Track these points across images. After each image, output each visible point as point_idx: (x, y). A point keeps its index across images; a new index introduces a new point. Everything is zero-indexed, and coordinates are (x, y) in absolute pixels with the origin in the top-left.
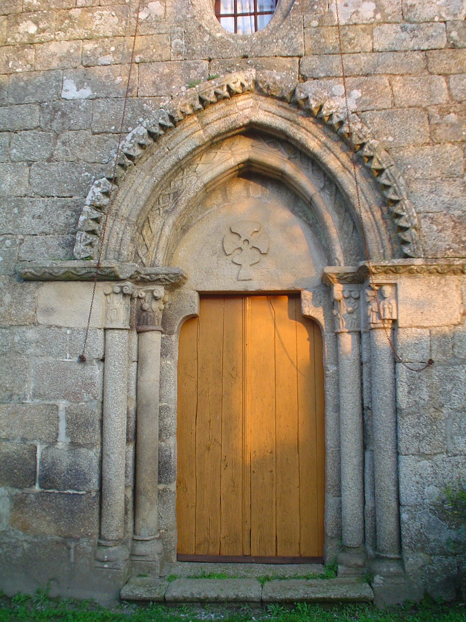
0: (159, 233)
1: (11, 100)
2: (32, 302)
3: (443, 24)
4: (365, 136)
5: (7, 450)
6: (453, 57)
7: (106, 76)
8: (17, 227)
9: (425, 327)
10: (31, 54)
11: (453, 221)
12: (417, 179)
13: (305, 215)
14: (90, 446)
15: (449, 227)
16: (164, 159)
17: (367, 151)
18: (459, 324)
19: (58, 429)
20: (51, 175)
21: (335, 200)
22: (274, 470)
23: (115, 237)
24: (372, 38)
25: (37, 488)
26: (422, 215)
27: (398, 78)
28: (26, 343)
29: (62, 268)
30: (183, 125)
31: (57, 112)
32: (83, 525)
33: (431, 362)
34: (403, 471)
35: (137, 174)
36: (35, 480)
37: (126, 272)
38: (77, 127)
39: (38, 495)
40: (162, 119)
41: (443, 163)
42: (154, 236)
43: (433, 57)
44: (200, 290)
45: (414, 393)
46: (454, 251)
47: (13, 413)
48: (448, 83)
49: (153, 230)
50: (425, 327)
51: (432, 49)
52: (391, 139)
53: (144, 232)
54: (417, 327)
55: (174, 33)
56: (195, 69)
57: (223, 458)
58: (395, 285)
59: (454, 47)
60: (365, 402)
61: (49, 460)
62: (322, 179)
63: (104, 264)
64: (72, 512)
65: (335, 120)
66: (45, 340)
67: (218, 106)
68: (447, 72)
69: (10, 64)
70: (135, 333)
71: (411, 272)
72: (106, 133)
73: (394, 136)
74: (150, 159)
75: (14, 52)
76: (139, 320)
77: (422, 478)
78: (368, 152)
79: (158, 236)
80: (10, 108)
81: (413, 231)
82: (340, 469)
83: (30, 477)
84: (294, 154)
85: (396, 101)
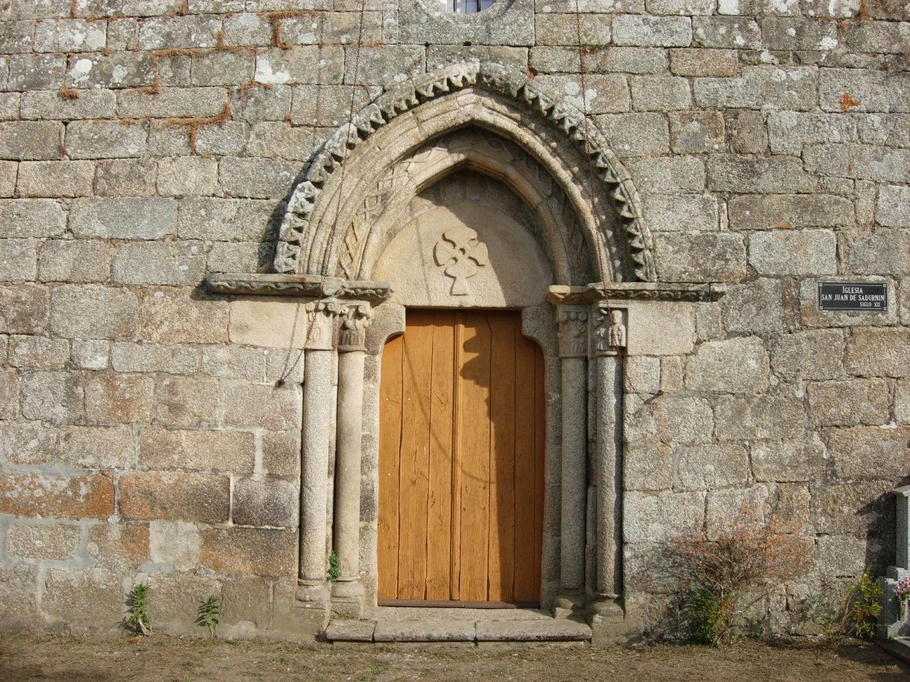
1: (195, 81)
2: (223, 318)
3: (689, 19)
4: (599, 145)
5: (196, 482)
6: (698, 58)
7: (306, 59)
8: (205, 232)
9: (656, 356)
10: (217, 26)
11: (690, 242)
12: (653, 194)
14: (290, 478)
15: (686, 248)
17: (600, 163)
18: (692, 353)
19: (254, 459)
20: (244, 172)
21: (564, 210)
22: (487, 507)
23: (319, 247)
24: (611, 29)
25: (230, 524)
26: (657, 234)
27: (638, 78)
28: (217, 363)
29: (261, 282)
31: (249, 98)
32: (282, 563)
33: (660, 393)
34: (627, 507)
36: (228, 514)
38: (274, 118)
39: (230, 531)
41: (683, 177)
43: (677, 57)
44: (408, 304)
45: (641, 427)
46: (690, 275)
47: (202, 442)
48: (692, 85)
49: (358, 237)
50: (656, 356)
51: (675, 47)
52: (627, 147)
53: (348, 240)
54: (647, 356)
55: (386, 11)
56: (410, 55)
57: (430, 493)
58: (624, 311)
59: (700, 46)
60: (590, 434)
61: (244, 493)
62: (550, 186)
63: (309, 279)
64: (270, 549)
65: (567, 125)
66: (239, 361)
67: (436, 101)
68: (691, 74)
69: (193, 37)
70: (336, 353)
71: (641, 296)
72: (308, 126)
73: (631, 145)
75: (198, 24)
76: (341, 338)
77: (646, 514)
80: (194, 91)
81: (647, 252)
82: (560, 505)
83: (223, 512)
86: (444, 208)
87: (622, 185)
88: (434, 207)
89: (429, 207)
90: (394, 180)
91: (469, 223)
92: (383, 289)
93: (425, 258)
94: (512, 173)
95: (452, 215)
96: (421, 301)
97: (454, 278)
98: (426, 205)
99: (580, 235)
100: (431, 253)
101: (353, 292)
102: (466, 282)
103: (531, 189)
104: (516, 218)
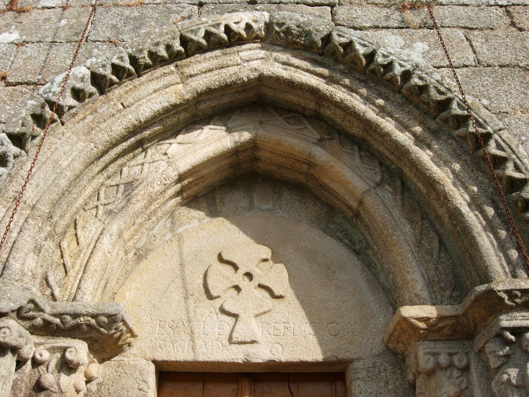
0: (92, 246)
7: (45, 20)
13: (347, 236)
16: (113, 119)
21: (403, 200)
27: (476, 32)
30: (152, 75)
35: (64, 138)
37: (9, 299)
40: (118, 58)
42: (80, 251)
44: (159, 358)
49: (81, 240)
62: (378, 169)
65: (398, 70)
73: (490, 99)
74: (90, 118)
78: (458, 110)
79: (90, 251)
84: (329, 134)
85: (481, 59)
86: (221, 219)
87: (496, 136)
88: (208, 219)
89: (199, 220)
90: (146, 166)
91: (260, 238)
92: (109, 316)
93: (189, 287)
94: (320, 154)
95: (234, 229)
96: (180, 353)
97: (236, 316)
98: (195, 220)
99: (433, 235)
100: (201, 281)
101: (57, 321)
102: (254, 323)
103: (348, 176)
104: (326, 230)
